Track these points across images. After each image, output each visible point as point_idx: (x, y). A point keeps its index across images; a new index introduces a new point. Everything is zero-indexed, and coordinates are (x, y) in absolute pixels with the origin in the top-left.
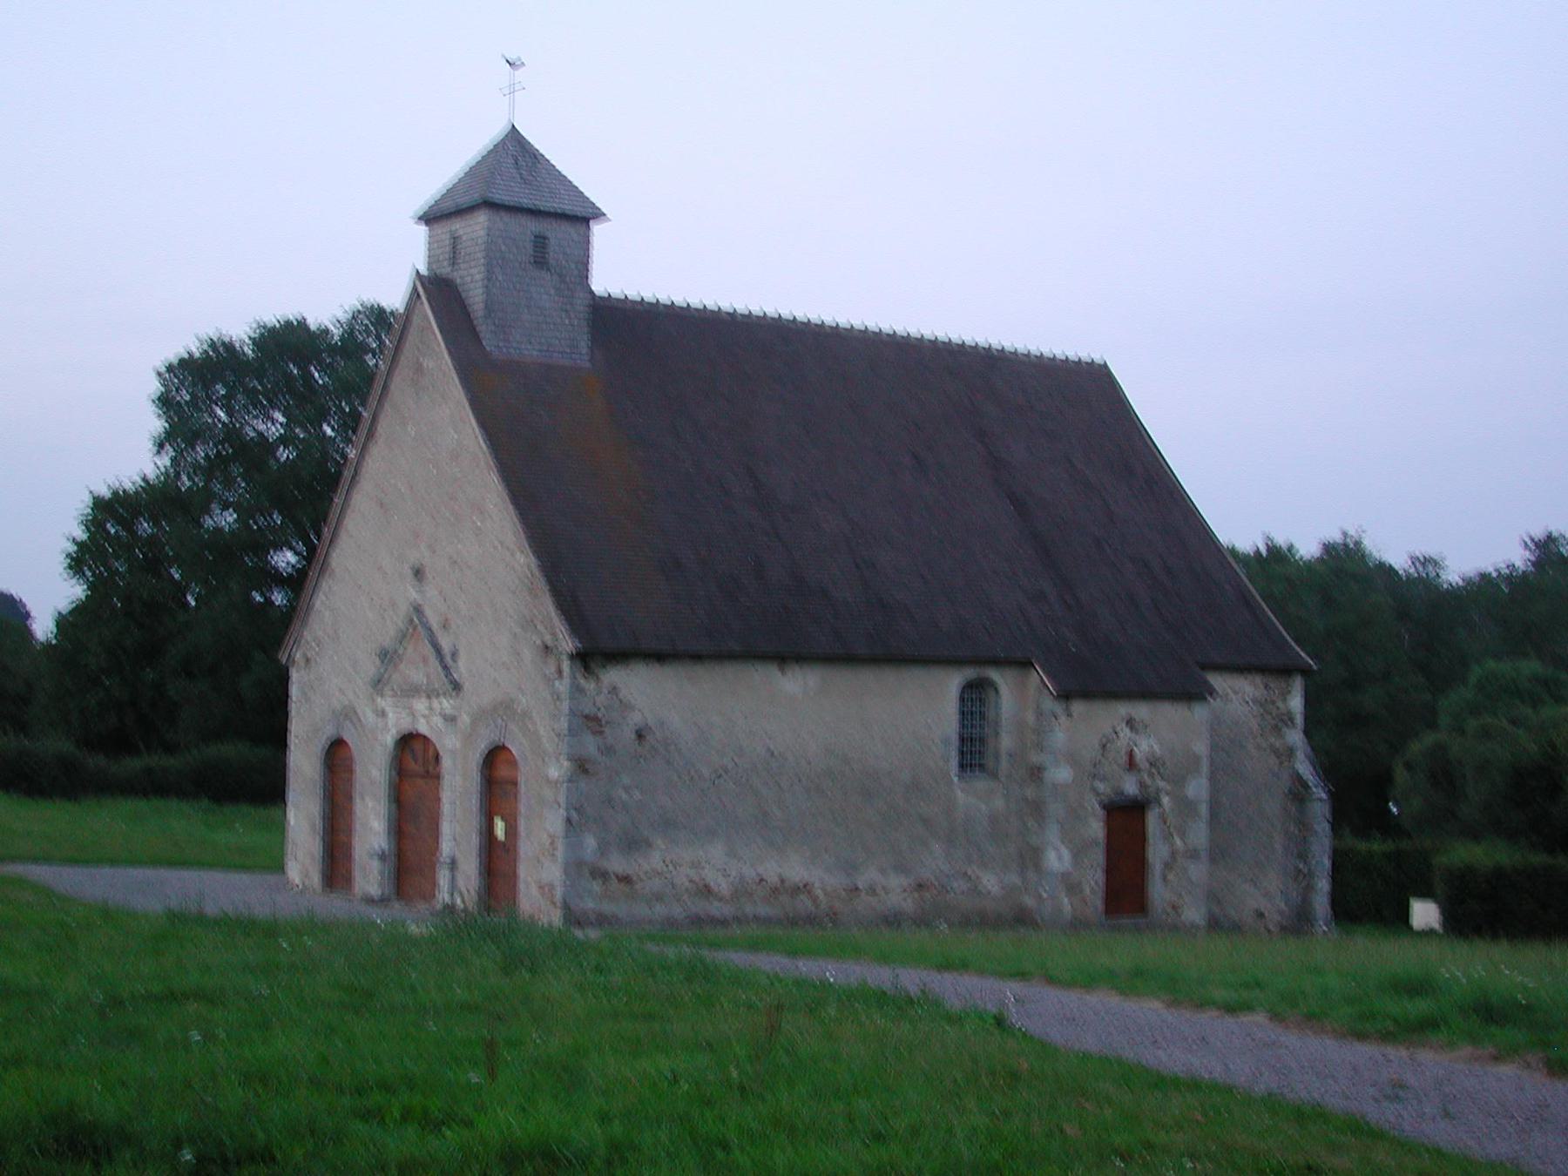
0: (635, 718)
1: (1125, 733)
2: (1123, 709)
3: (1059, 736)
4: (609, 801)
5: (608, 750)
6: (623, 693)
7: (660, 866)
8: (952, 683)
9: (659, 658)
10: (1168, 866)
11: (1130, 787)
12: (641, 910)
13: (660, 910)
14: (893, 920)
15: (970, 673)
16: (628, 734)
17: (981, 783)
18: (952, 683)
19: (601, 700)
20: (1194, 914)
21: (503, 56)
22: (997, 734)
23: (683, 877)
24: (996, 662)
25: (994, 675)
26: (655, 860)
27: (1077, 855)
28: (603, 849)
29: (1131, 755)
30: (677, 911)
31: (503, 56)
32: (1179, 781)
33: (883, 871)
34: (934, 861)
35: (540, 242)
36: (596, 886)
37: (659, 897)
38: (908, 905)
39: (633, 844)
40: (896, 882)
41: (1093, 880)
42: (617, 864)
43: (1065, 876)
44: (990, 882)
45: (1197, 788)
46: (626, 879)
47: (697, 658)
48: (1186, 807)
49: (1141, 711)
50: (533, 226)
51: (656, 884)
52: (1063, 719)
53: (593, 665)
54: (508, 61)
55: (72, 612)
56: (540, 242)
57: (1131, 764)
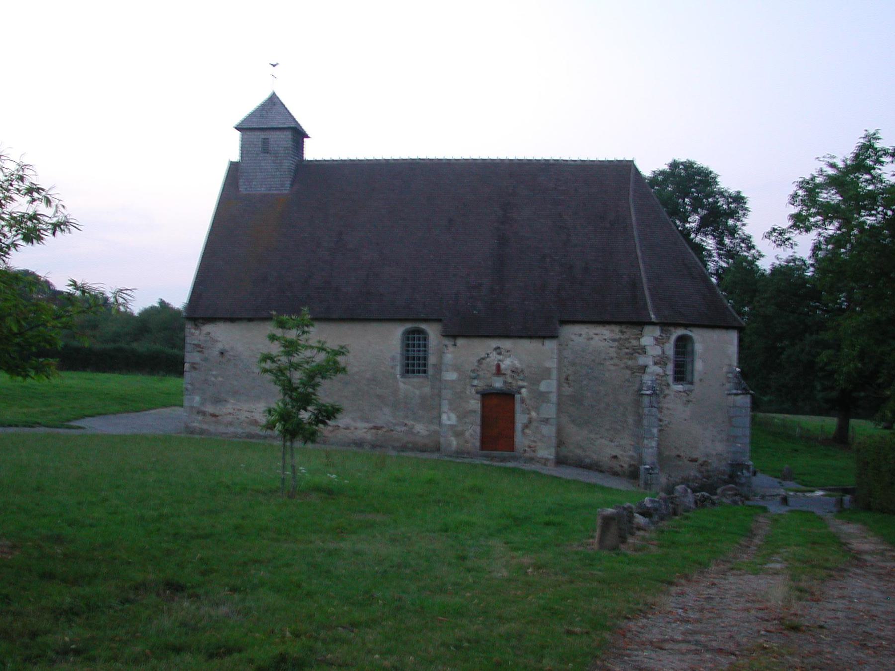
0: (220, 346)
1: (494, 356)
2: (494, 343)
3: (449, 357)
4: (206, 381)
5: (206, 360)
6: (213, 335)
7: (231, 410)
8: (397, 331)
9: (232, 320)
10: (526, 426)
11: (498, 384)
12: (222, 429)
13: (231, 430)
14: (360, 444)
15: (409, 325)
16: (216, 353)
17: (415, 380)
18: (397, 331)
19: (202, 338)
20: (546, 452)
21: (270, 64)
22: (692, 361)
23: (243, 416)
24: (425, 320)
25: (423, 326)
26: (229, 408)
27: (462, 417)
28: (204, 401)
29: (498, 366)
30: (240, 431)
31: (270, 64)
32: (535, 381)
33: (354, 420)
34: (385, 417)
35: (265, 141)
36: (200, 418)
37: (231, 424)
38: (369, 437)
39: (218, 400)
40: (361, 425)
41: (473, 431)
42: (210, 409)
43: (452, 427)
44: (420, 429)
45: (549, 386)
46: (214, 415)
47: (250, 320)
48: (543, 397)
49: (506, 344)
50: (262, 135)
51: (229, 418)
52: (451, 349)
53: (199, 324)
54: (272, 65)
55: (189, 302)
56: (265, 141)
57: (499, 371)
